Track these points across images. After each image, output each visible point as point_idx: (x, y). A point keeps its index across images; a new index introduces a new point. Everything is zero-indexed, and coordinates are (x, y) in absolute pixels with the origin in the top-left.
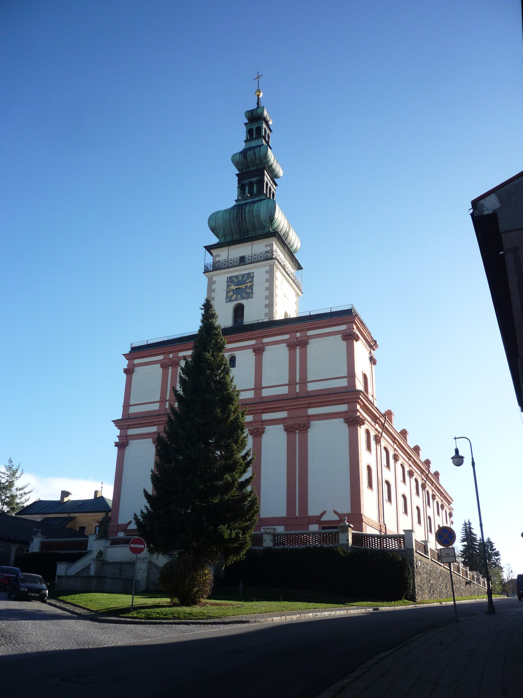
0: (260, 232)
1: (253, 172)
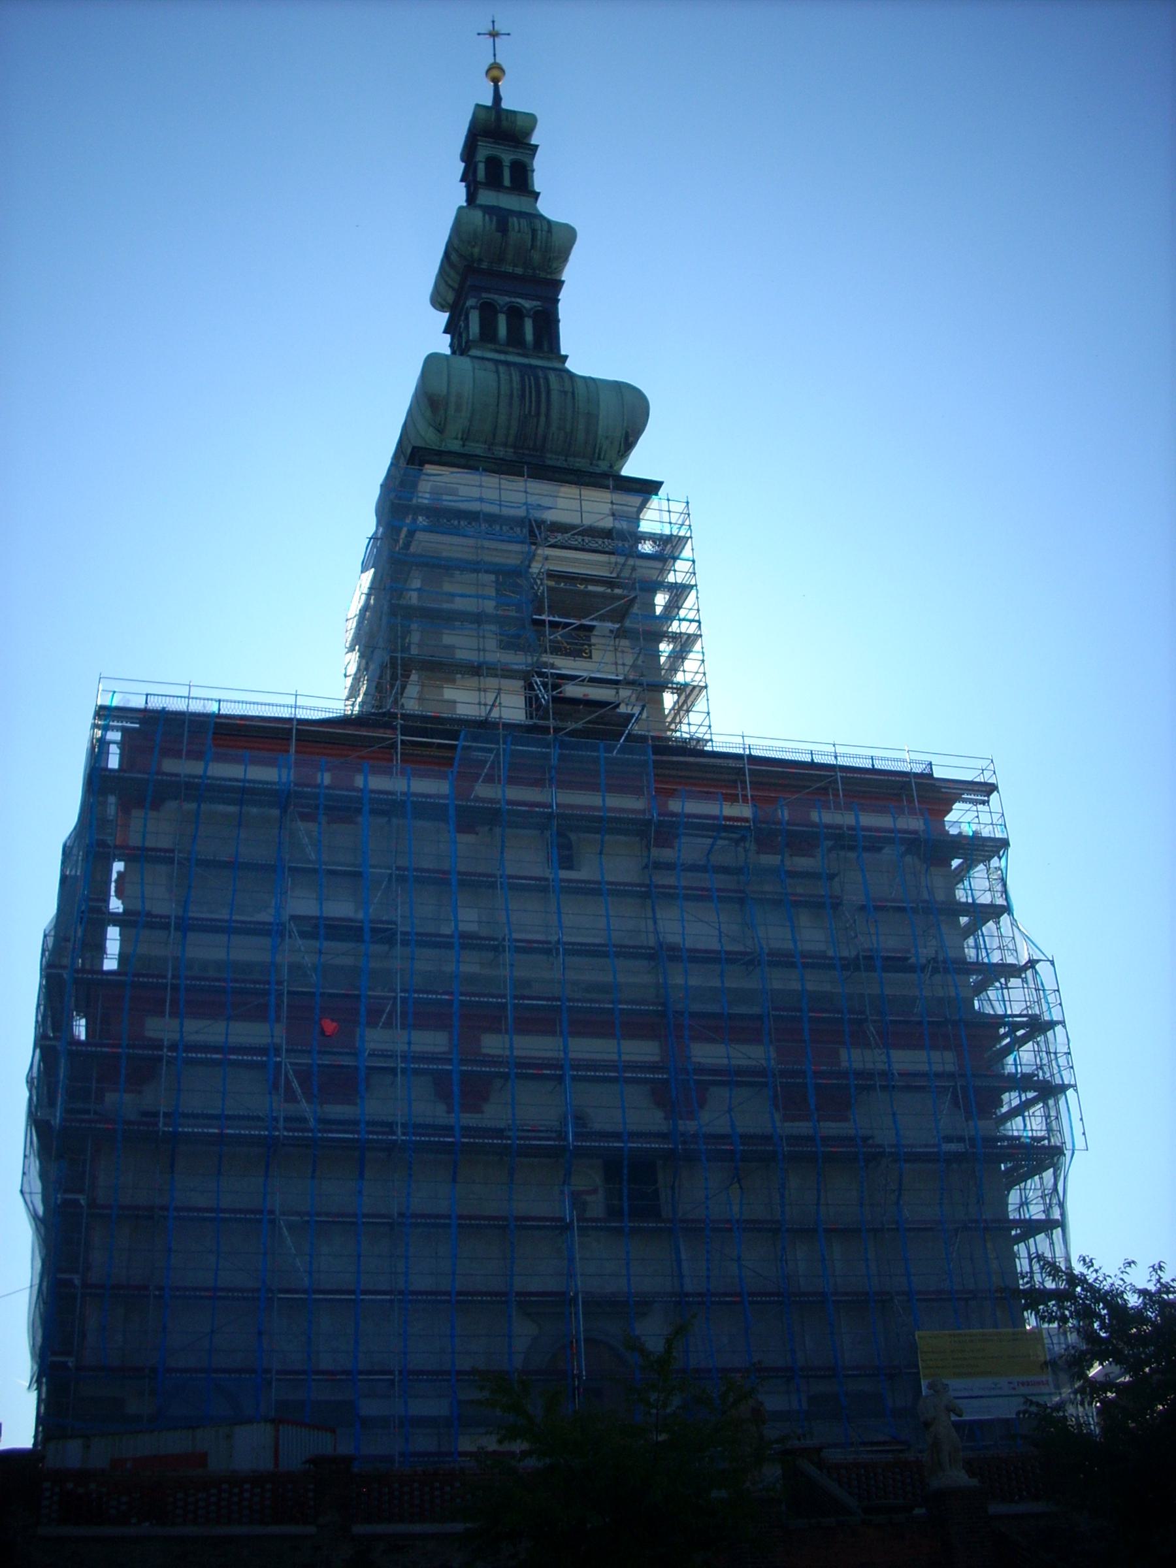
0: (580, 463)
1: (502, 275)
